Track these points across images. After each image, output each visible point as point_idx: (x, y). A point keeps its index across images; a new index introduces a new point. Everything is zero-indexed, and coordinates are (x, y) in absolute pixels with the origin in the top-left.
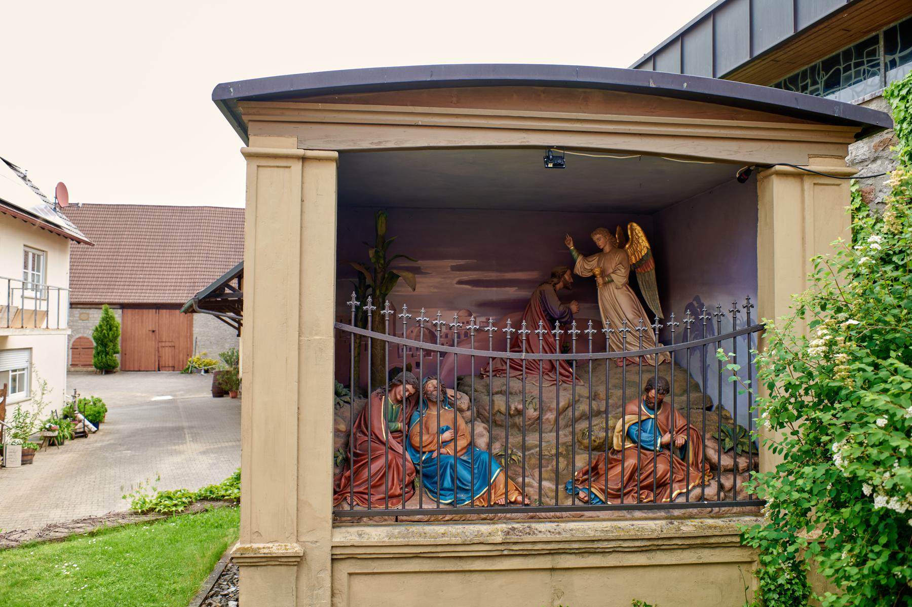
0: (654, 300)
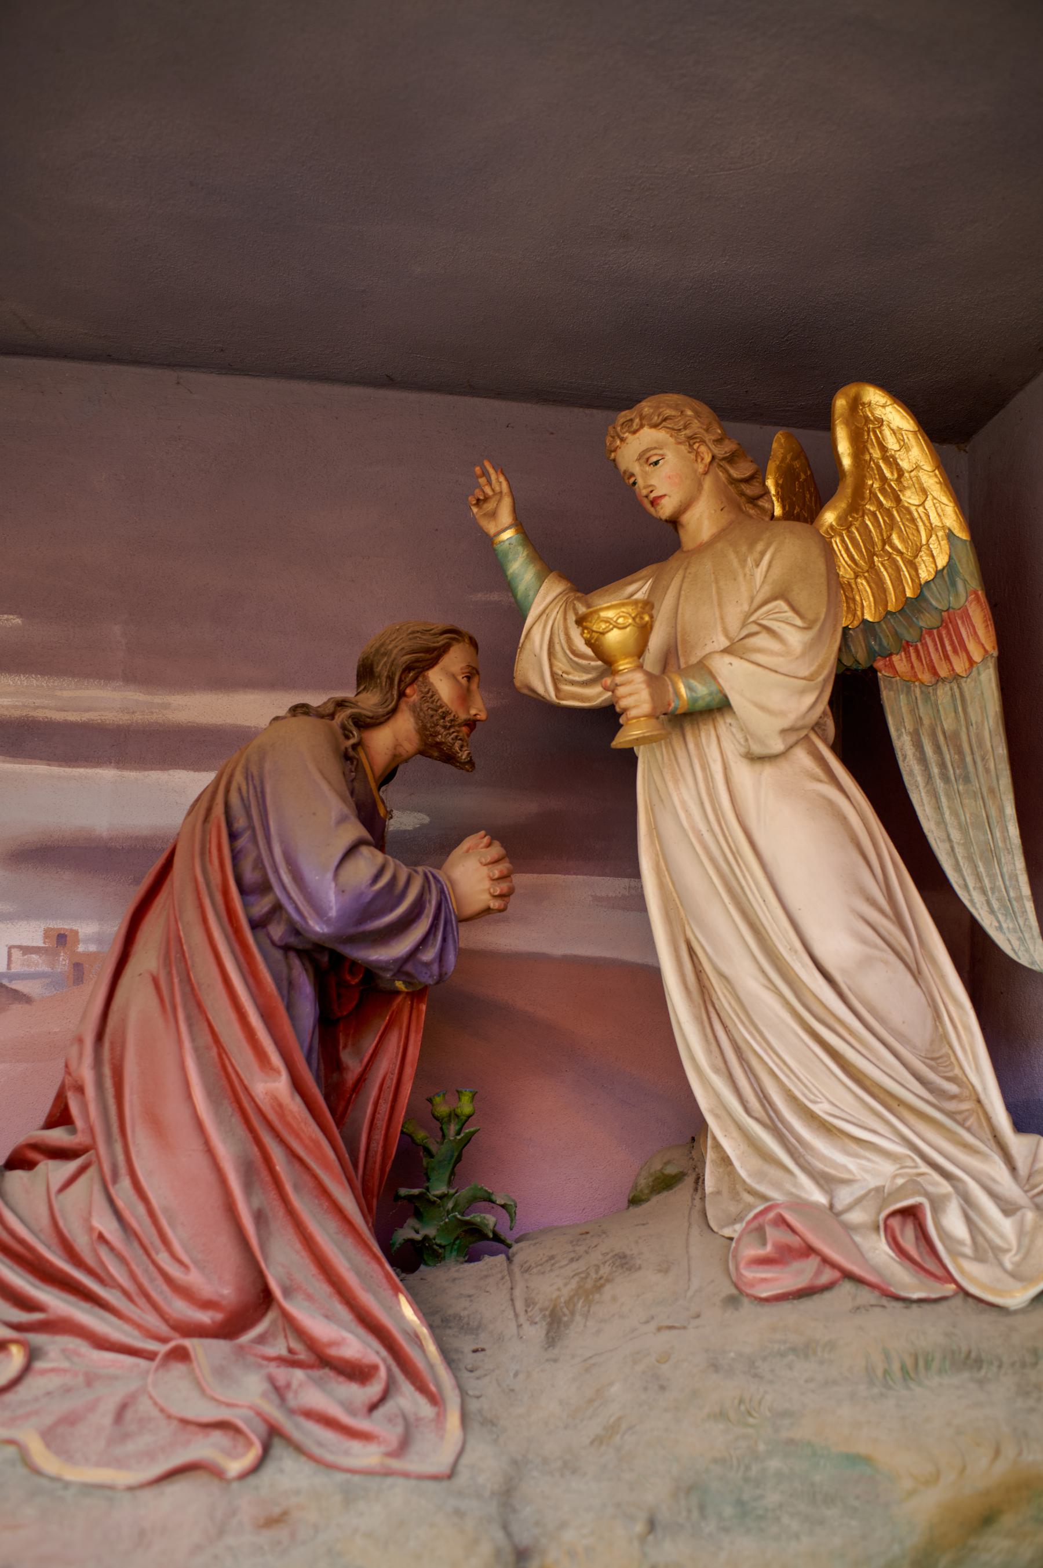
0: (991, 855)
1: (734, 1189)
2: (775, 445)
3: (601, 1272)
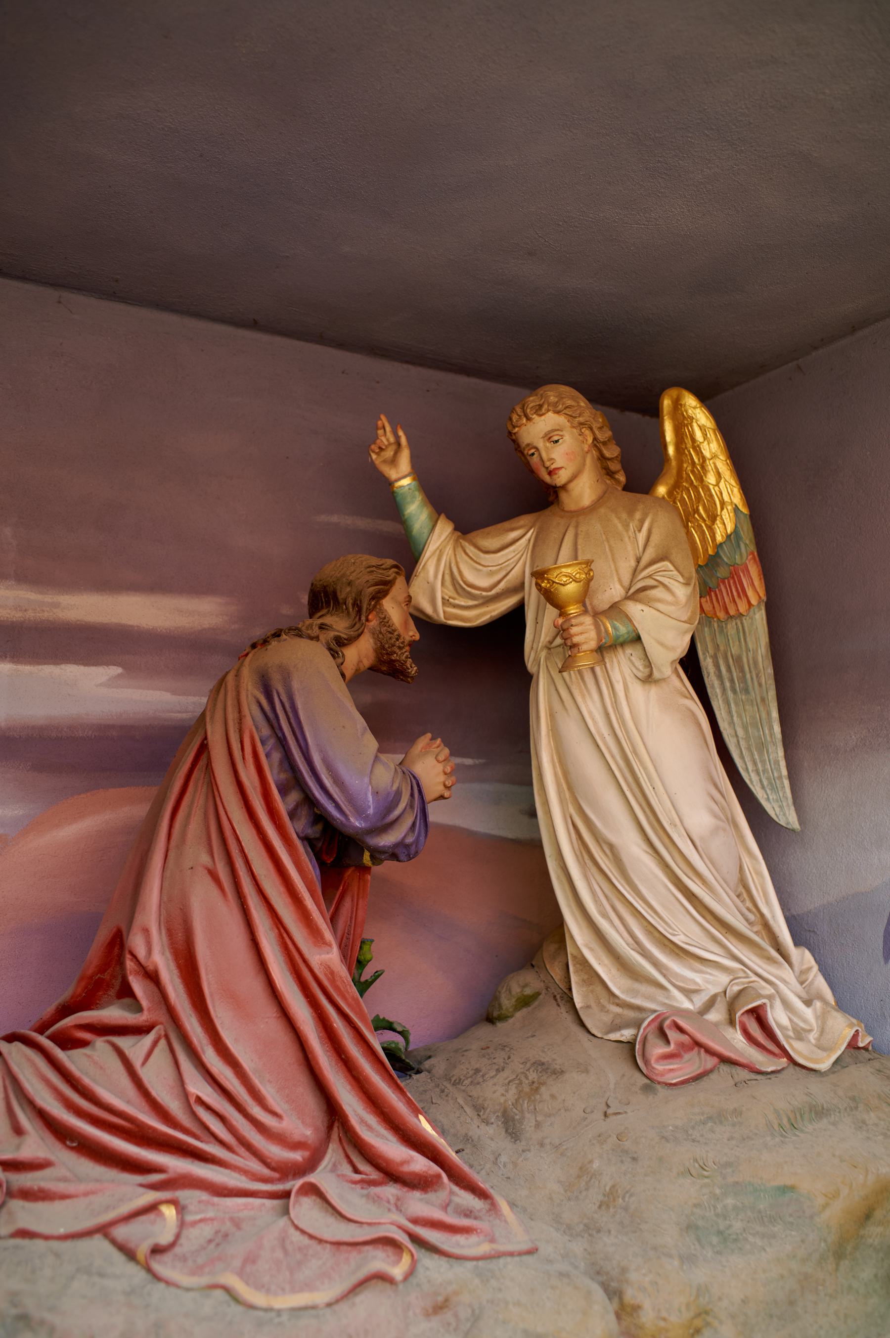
0: (762, 746)
1: (600, 1003)
3: (530, 1078)
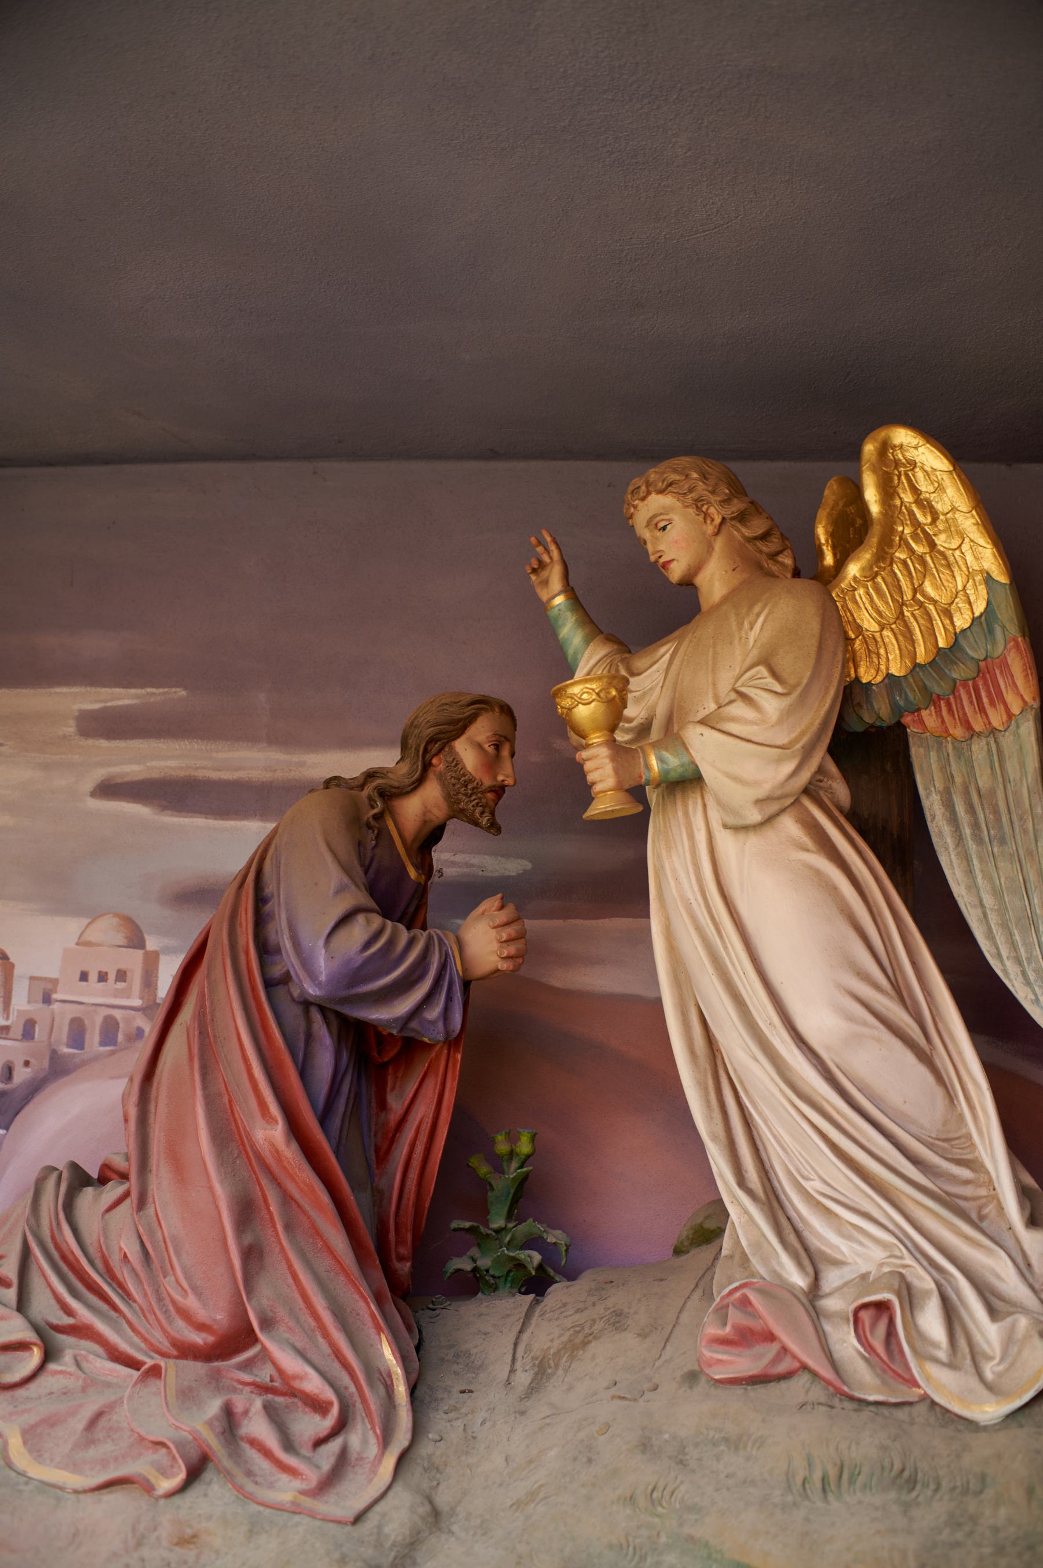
2: (827, 492)
